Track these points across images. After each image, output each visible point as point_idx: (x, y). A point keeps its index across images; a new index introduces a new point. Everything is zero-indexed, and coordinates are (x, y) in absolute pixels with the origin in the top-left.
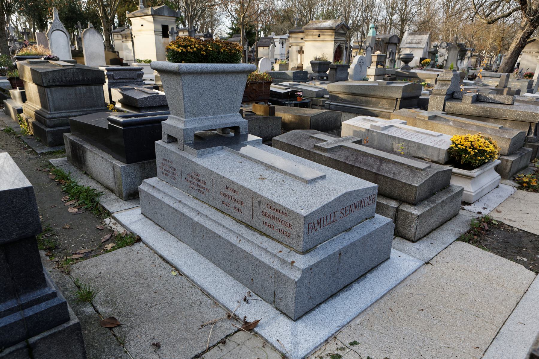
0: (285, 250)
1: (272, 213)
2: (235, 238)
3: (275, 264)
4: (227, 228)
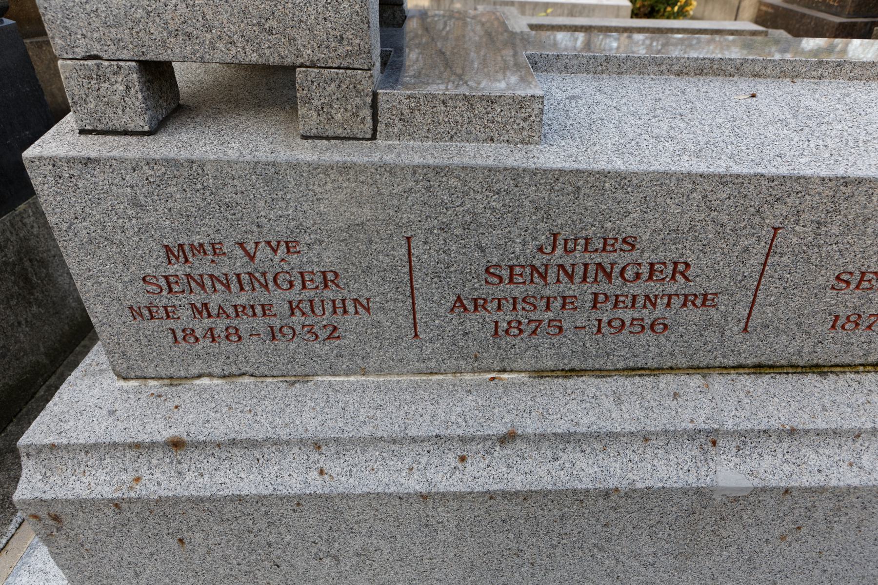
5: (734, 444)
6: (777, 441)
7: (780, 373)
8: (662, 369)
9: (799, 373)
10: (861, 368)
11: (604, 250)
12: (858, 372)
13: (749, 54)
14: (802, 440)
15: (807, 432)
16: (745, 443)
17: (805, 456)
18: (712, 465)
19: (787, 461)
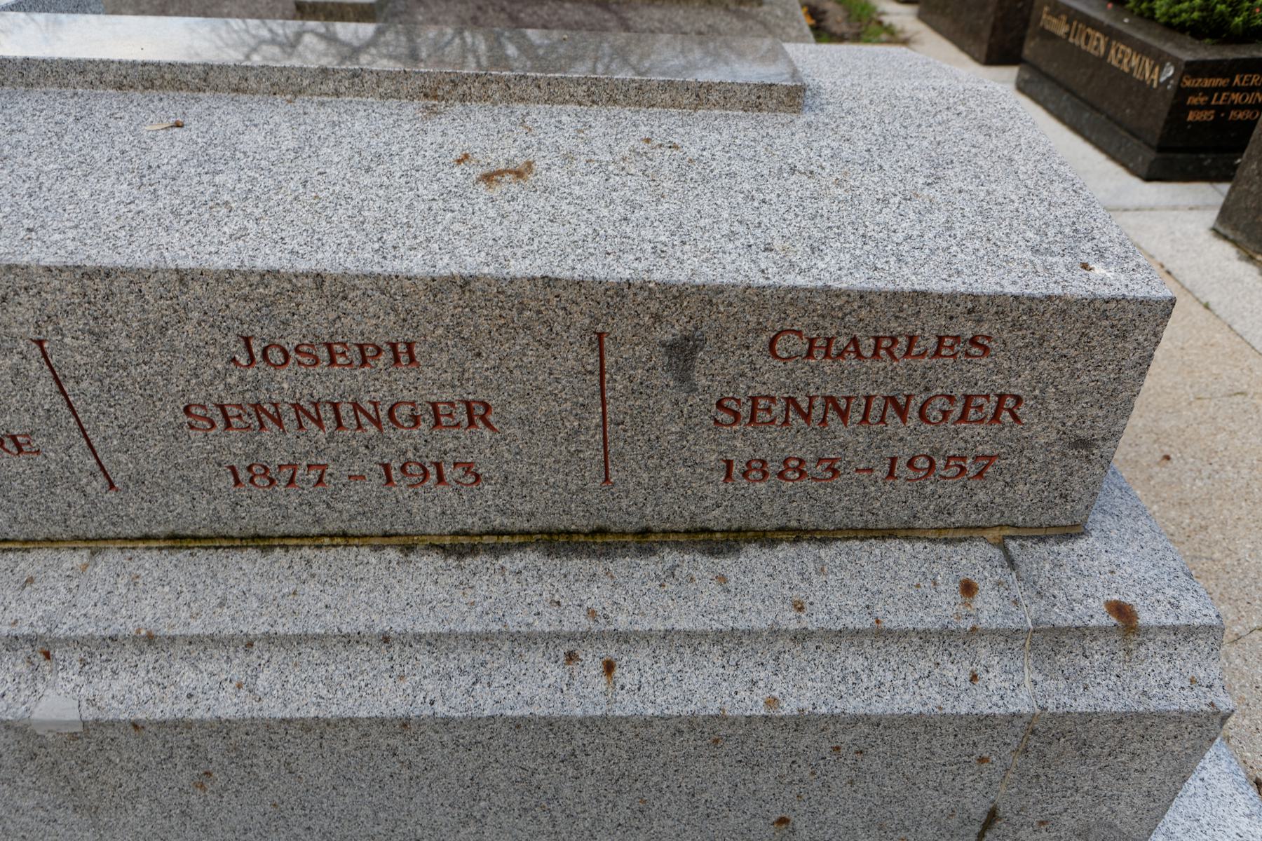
0: (975, 558)
1: (826, 379)
2: (556, 673)
3: (994, 680)
4: (433, 642)
5: (76, 656)
6: (137, 652)
7: (207, 548)
8: (34, 541)
9: (237, 547)
10: (327, 541)
11: (937, 353)
12: (319, 547)
13: (533, 69)
14: (172, 650)
15: (173, 639)
16: (92, 655)
17: (178, 673)
18: (40, 687)
19: (150, 682)
